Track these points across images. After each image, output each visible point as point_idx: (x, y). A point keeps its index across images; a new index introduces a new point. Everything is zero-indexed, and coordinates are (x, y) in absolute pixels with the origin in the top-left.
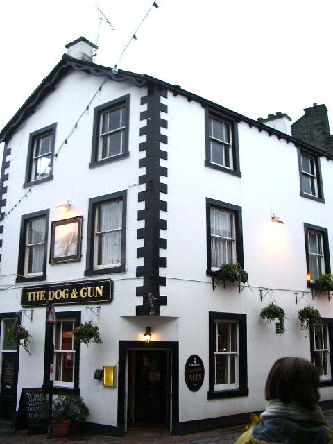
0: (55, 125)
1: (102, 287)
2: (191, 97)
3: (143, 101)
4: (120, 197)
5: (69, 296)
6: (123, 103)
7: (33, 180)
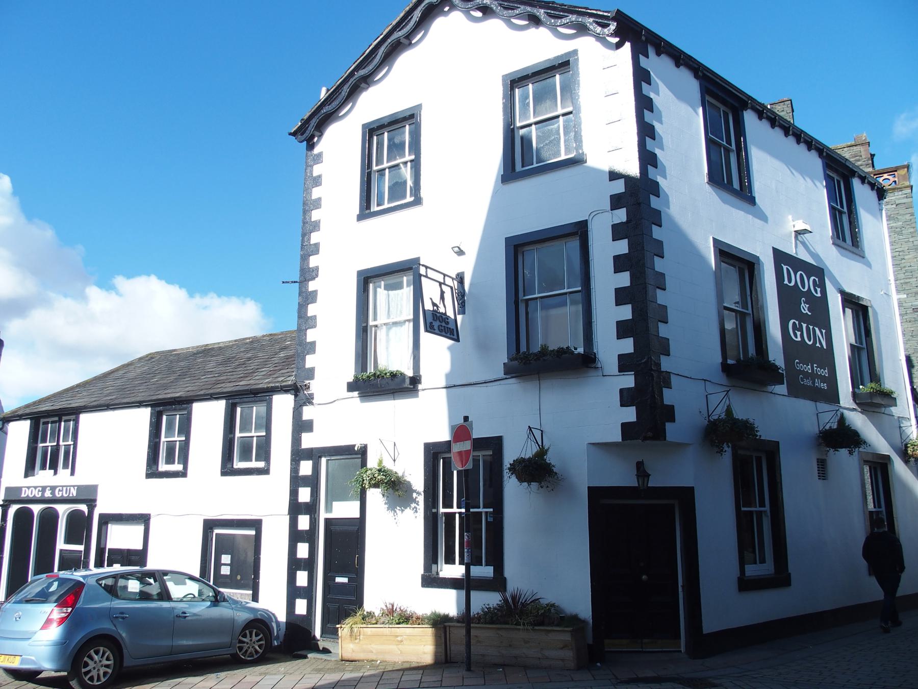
0: (419, 107)
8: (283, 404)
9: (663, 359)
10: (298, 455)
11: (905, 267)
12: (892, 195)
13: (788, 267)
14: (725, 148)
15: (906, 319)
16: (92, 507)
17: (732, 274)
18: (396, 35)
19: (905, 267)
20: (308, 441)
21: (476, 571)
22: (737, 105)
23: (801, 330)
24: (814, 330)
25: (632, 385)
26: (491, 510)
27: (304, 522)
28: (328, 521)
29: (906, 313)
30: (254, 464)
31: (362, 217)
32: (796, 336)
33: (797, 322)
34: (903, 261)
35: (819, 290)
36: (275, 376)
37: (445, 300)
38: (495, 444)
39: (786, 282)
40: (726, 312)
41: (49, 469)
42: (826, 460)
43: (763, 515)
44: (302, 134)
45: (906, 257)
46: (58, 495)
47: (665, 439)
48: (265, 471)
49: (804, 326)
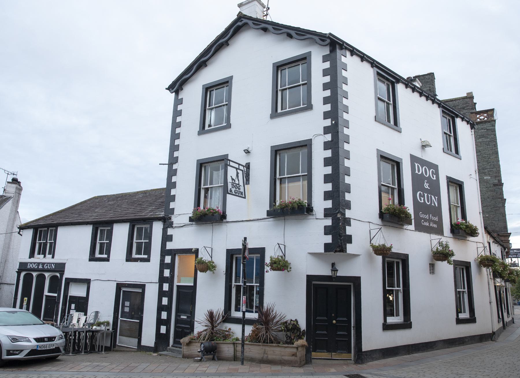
0: (231, 78)
2: (363, 57)
3: (325, 59)
4: (306, 145)
6: (305, 59)
7: (207, 128)
8: (157, 228)
9: (347, 211)
10: (164, 252)
11: (490, 162)
12: (485, 124)
13: (418, 164)
14: (387, 103)
15: (490, 189)
16: (62, 274)
17: (387, 167)
18: (221, 41)
19: (490, 162)
20: (170, 246)
21: (248, 315)
22: (394, 81)
23: (424, 196)
24: (431, 197)
25: (331, 224)
26: (258, 285)
27: (166, 287)
28: (178, 287)
29: (490, 187)
30: (142, 256)
31: (200, 133)
32: (421, 200)
33: (422, 193)
34: (489, 159)
35: (435, 176)
36: (155, 211)
37: (239, 177)
38: (261, 251)
39: (417, 172)
40: (382, 187)
41: (42, 254)
42: (434, 264)
43: (399, 292)
44: (173, 89)
45: (491, 157)
46: (46, 267)
47: (346, 252)
48: (148, 260)
49: (426, 195)
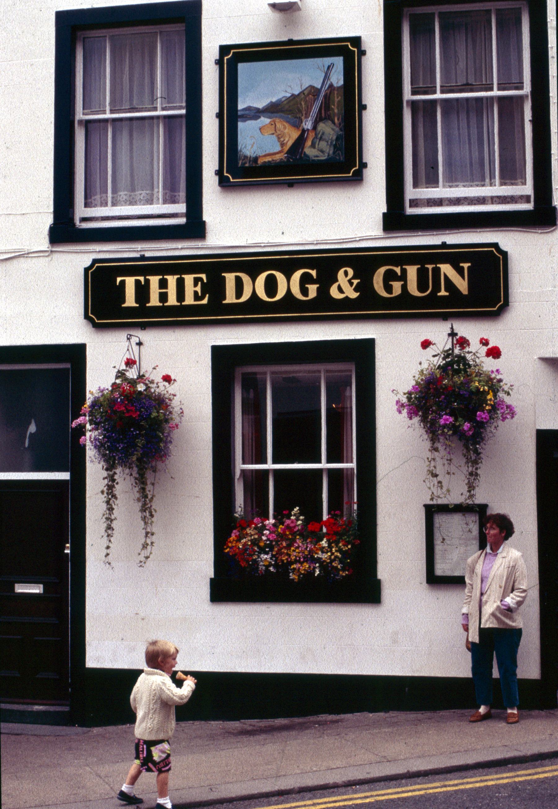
1: (466, 265)
5: (323, 292)
